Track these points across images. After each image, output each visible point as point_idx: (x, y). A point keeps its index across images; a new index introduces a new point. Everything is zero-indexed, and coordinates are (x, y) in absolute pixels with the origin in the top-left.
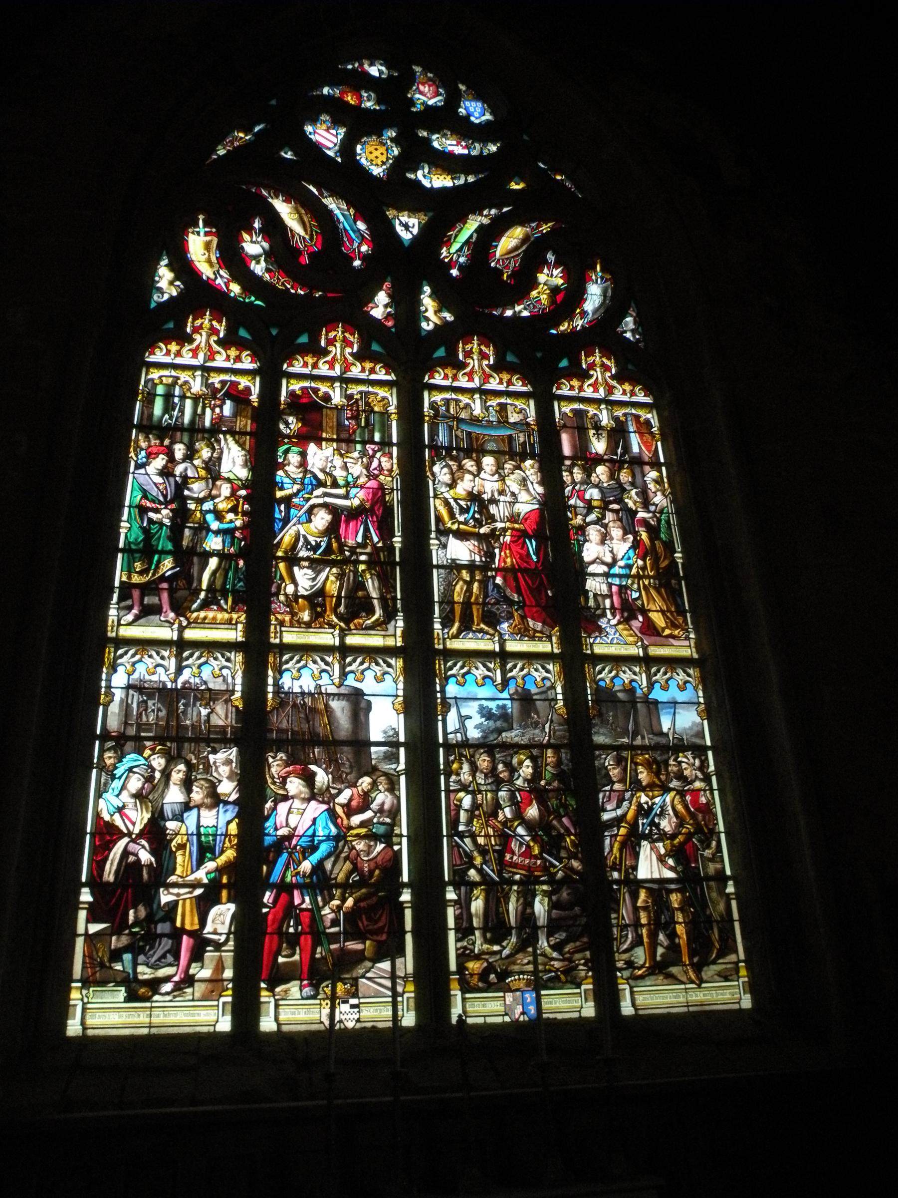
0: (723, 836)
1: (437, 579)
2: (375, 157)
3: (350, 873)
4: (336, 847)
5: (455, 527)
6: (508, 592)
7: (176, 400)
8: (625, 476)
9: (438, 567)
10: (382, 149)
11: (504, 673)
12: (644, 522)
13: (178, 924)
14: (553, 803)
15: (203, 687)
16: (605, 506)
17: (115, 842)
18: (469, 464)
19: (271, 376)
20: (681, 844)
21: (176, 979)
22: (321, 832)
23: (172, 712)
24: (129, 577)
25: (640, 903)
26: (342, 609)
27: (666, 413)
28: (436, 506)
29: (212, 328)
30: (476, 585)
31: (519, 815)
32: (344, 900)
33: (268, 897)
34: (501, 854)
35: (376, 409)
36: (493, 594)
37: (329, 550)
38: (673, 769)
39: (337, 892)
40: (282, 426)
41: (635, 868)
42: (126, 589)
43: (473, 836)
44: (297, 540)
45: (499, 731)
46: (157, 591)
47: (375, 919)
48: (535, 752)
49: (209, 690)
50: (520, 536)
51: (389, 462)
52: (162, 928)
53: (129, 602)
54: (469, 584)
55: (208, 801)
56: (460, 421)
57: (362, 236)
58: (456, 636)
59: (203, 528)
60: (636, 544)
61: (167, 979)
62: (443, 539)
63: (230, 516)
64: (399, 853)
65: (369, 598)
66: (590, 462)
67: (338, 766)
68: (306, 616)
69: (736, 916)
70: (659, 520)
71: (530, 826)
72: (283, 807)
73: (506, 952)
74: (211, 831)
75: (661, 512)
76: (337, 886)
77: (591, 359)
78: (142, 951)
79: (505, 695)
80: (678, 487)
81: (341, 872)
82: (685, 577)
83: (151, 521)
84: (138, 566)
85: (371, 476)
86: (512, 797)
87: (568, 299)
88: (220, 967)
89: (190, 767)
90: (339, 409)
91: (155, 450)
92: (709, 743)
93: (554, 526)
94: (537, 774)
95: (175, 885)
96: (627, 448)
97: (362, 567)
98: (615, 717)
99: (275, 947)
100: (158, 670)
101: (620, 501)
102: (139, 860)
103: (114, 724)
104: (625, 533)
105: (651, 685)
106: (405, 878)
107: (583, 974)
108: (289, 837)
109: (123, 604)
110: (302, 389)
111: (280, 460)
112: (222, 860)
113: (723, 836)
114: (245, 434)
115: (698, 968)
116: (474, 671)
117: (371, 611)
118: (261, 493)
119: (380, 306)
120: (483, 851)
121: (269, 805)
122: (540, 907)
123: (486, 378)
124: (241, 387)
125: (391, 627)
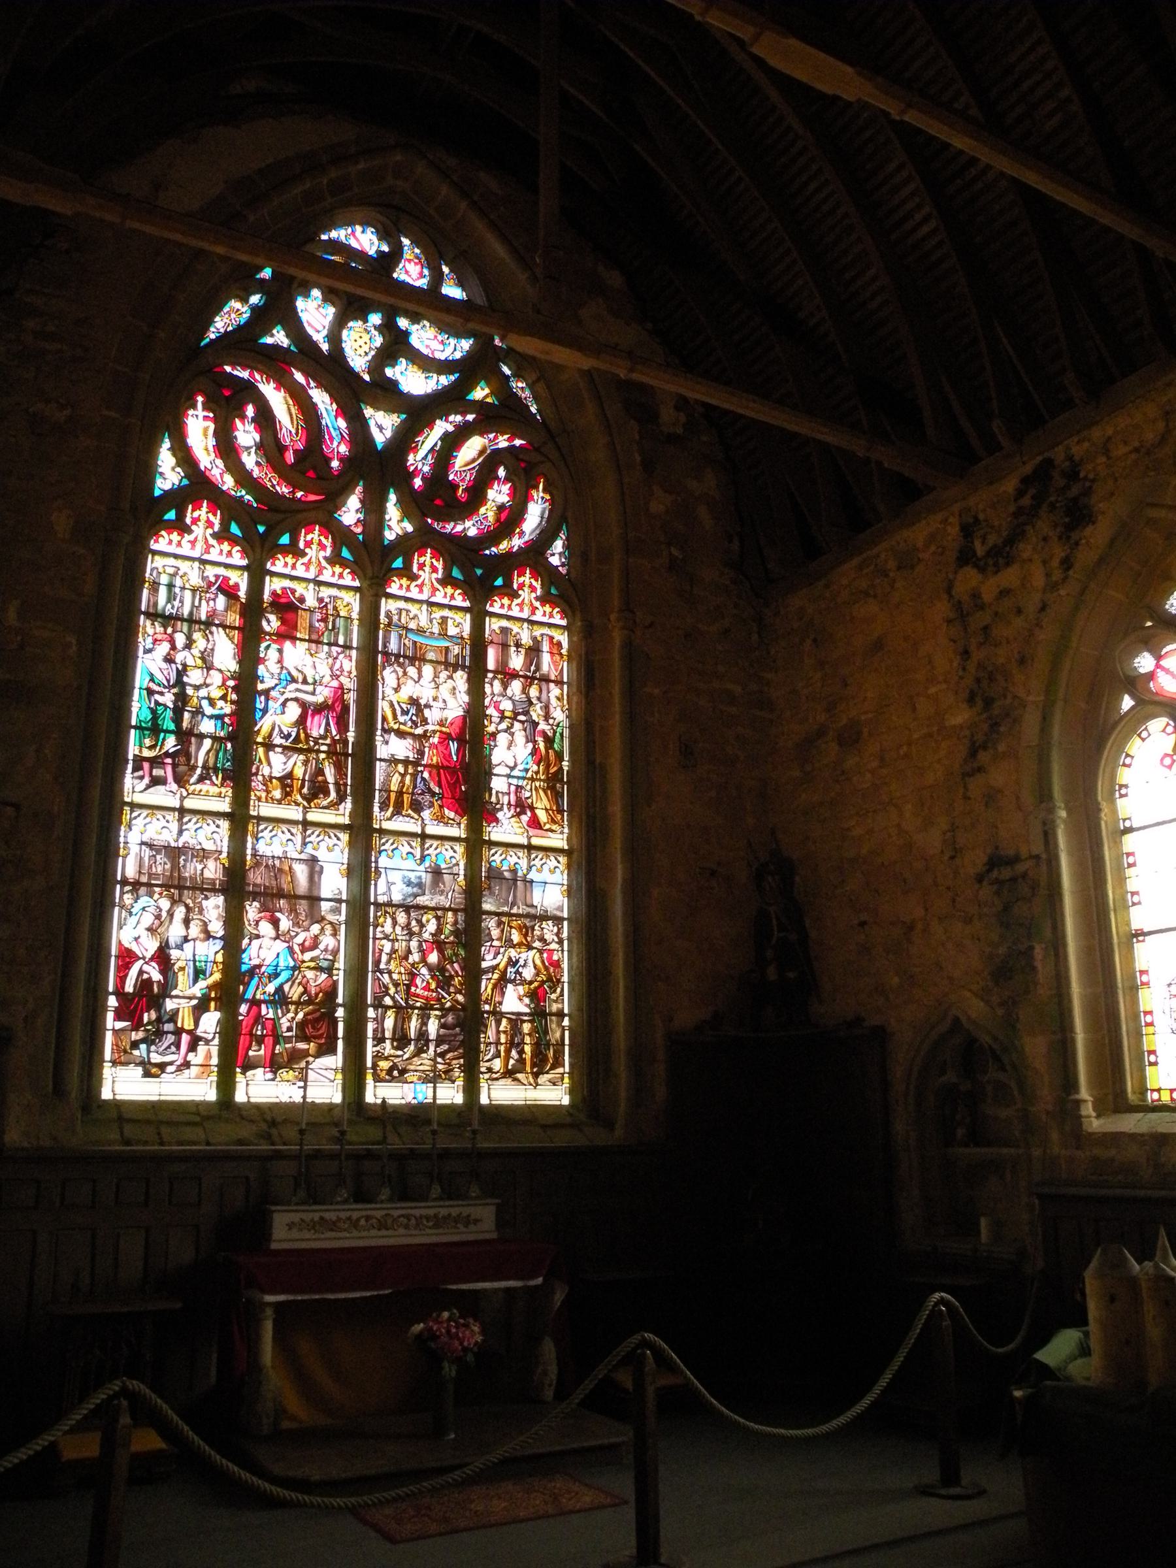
0: (566, 985)
1: (380, 769)
2: (360, 344)
3: (302, 994)
4: (293, 975)
5: (396, 727)
6: (432, 785)
7: (177, 590)
8: (534, 692)
9: (381, 760)
10: (366, 337)
11: (423, 850)
12: (544, 734)
13: (179, 1025)
14: (449, 952)
15: (199, 847)
16: (514, 718)
17: (133, 963)
18: (412, 671)
19: (257, 574)
20: (536, 988)
21: (178, 1063)
22: (282, 964)
23: (175, 866)
24: (141, 751)
25: (502, 1028)
26: (305, 791)
27: (575, 639)
28: (383, 707)
29: (208, 521)
30: (408, 778)
31: (424, 960)
32: (296, 1014)
33: (243, 1008)
34: (408, 987)
35: (342, 614)
36: (420, 785)
37: (297, 740)
38: (537, 932)
39: (292, 1008)
40: (264, 623)
41: (501, 1003)
42: (139, 762)
43: (390, 973)
44: (273, 729)
45: (416, 896)
46: (162, 765)
47: (318, 1027)
48: (440, 913)
49: (203, 850)
50: (446, 738)
51: (349, 664)
52: (168, 1027)
53: (140, 773)
54: (403, 776)
55: (202, 936)
56: (408, 630)
57: (342, 436)
58: (389, 819)
59: (198, 712)
60: (535, 752)
61: (171, 1063)
62: (386, 736)
63: (221, 703)
64: (335, 983)
65: (326, 782)
66: (508, 675)
67: (297, 915)
68: (277, 794)
69: (567, 1042)
70: (555, 732)
71: (430, 969)
72: (256, 943)
73: (406, 1057)
74: (203, 959)
75: (558, 725)
76: (292, 1003)
77: (521, 580)
78: (153, 1042)
79: (422, 868)
80: (574, 707)
81: (295, 993)
82: (568, 783)
83: (157, 703)
84: (148, 742)
85: (335, 677)
86: (420, 946)
87: (510, 519)
88: (209, 1056)
89: (189, 909)
90: (311, 611)
91: (159, 637)
92: (566, 916)
93: (472, 732)
94: (439, 930)
95: (177, 997)
96: (538, 668)
97: (322, 756)
98: (500, 890)
99: (247, 1043)
100: (163, 830)
101: (526, 713)
102: (150, 978)
103: (131, 872)
104: (527, 742)
105: (530, 868)
106: (340, 1000)
107: (457, 1074)
108: (259, 966)
109: (136, 774)
110: (284, 589)
111: (262, 655)
112: (210, 981)
113: (566, 985)
114: (234, 628)
115: (536, 1075)
116: (400, 847)
117: (327, 793)
118: (245, 685)
119: (351, 512)
120: (396, 985)
121: (246, 941)
122: (433, 1027)
123: (434, 590)
124: (231, 583)
125: (342, 807)
